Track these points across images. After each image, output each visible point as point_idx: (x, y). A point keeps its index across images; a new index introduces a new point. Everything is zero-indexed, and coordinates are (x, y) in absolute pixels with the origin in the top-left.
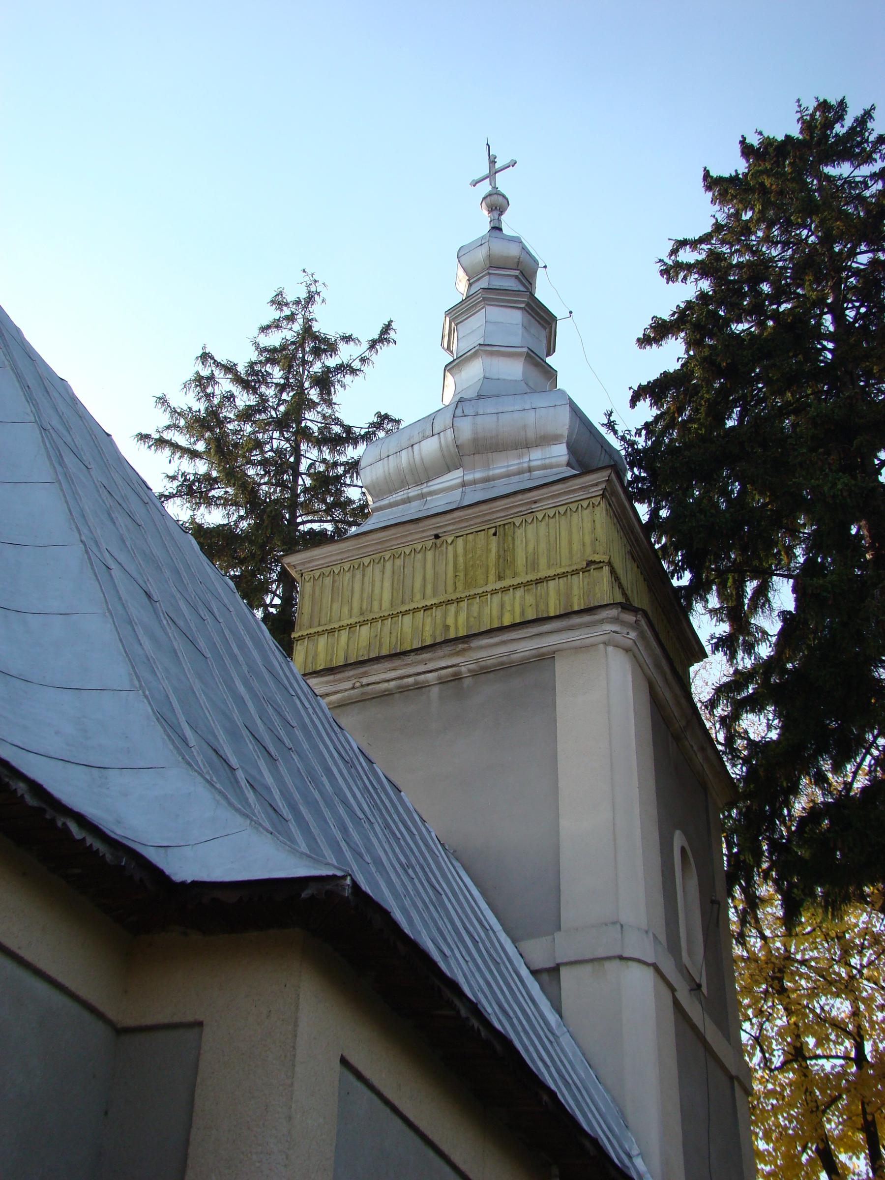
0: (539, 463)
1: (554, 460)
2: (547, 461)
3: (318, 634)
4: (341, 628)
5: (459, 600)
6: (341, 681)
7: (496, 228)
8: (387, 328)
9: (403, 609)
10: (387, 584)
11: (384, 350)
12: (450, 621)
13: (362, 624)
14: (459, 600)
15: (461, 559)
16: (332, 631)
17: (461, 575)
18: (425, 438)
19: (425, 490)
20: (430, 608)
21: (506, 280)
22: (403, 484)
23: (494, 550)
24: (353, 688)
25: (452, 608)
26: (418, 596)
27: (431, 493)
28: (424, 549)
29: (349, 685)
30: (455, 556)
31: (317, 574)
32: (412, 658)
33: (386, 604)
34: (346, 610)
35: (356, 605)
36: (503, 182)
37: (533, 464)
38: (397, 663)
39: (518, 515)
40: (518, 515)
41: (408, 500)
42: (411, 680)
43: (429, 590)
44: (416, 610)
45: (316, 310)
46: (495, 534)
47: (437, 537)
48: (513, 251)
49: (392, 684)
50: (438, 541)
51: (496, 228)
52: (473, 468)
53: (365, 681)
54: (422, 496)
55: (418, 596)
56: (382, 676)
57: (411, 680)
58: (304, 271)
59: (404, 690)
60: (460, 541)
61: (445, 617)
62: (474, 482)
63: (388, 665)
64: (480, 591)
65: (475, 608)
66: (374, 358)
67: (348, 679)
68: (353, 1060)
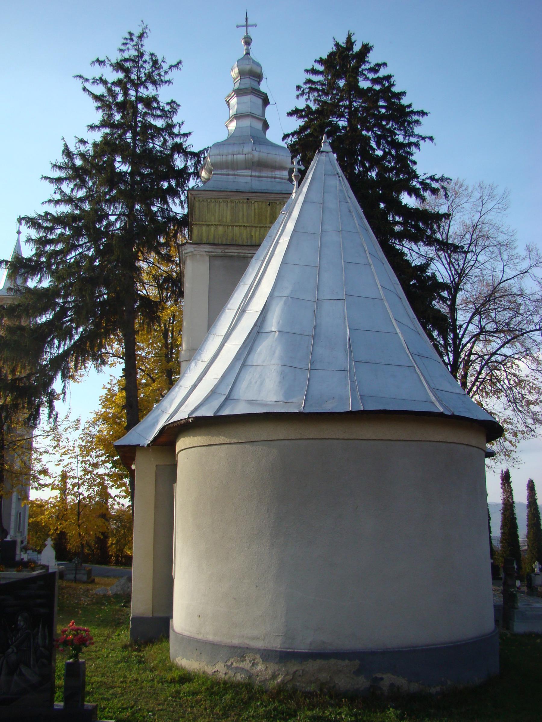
0: (279, 176)
1: (284, 177)
2: (281, 176)
3: (203, 225)
4: (212, 225)
5: (256, 227)
6: (217, 249)
7: (248, 54)
8: (179, 63)
9: (236, 224)
10: (229, 213)
11: (174, 70)
12: (253, 234)
13: (220, 225)
14: (256, 227)
15: (257, 211)
16: (208, 225)
17: (257, 217)
18: (239, 154)
19: (236, 173)
20: (246, 227)
21: (251, 80)
22: (227, 168)
23: (269, 211)
24: (222, 252)
25: (254, 229)
26: (241, 221)
27: (238, 175)
28: (243, 203)
29: (220, 251)
30: (255, 209)
31: (201, 200)
32: (245, 247)
33: (229, 220)
34: (213, 218)
35: (216, 217)
36: (252, 32)
37: (277, 176)
38: (239, 248)
39: (278, 200)
40: (278, 200)
41: (228, 175)
42: (243, 254)
43: (245, 219)
44: (240, 226)
45: (145, 41)
46: (269, 205)
47: (248, 199)
48: (259, 71)
49: (236, 254)
50: (248, 201)
51: (248, 54)
52: (255, 171)
53: (226, 251)
54: (234, 175)
55: (241, 221)
56: (233, 251)
57: (243, 254)
58: (142, 21)
59: (239, 257)
60: (256, 204)
61: (251, 231)
62: (255, 176)
63: (236, 248)
64: (264, 226)
65: (262, 231)
66: (170, 72)
67: (220, 249)
68: (513, 479)
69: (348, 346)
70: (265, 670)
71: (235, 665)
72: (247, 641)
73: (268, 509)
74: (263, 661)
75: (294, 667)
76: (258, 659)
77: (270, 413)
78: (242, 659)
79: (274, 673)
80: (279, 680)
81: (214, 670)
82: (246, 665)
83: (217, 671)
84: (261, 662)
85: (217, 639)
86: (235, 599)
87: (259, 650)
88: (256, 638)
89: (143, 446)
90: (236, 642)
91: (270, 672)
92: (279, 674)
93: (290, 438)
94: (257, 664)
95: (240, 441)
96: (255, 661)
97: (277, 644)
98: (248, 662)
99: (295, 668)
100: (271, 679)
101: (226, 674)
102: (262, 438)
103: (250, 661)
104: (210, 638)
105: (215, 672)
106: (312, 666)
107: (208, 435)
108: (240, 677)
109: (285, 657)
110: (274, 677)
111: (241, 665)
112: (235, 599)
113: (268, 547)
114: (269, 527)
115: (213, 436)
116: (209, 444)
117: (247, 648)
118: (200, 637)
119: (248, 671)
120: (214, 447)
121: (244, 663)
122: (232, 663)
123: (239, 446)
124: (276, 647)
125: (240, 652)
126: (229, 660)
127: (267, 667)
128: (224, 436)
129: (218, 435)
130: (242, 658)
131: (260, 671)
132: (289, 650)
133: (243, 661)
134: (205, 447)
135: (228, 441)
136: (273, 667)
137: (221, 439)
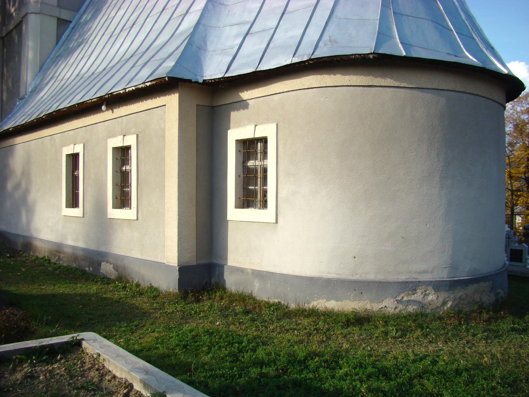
69: (463, 17)
70: (437, 299)
71: (405, 298)
72: (415, 276)
73: (438, 154)
74: (435, 291)
75: (460, 293)
76: (430, 290)
77: (443, 61)
78: (414, 292)
79: (445, 300)
80: (449, 306)
81: (380, 307)
82: (418, 296)
83: (385, 307)
84: (433, 292)
85: (381, 277)
86: (403, 238)
87: (431, 282)
88: (424, 272)
89: (197, 82)
90: (403, 278)
91: (441, 300)
92: (448, 301)
93: (457, 90)
94: (428, 295)
95: (410, 86)
96: (427, 292)
97: (443, 275)
98: (419, 294)
99: (460, 294)
100: (441, 306)
101: (395, 308)
102: (433, 87)
103: (422, 293)
104: (371, 277)
105: (382, 308)
106: (471, 289)
107: (369, 75)
108: (411, 309)
109: (452, 285)
110: (444, 303)
111: (413, 298)
112: (403, 238)
113: (437, 189)
114: (439, 170)
115: (377, 77)
116: (370, 84)
117: (419, 282)
118: (356, 277)
119: (420, 302)
120: (374, 88)
121: (415, 295)
122: (403, 298)
123: (408, 91)
124: (443, 278)
125: (411, 286)
126: (400, 295)
127: (438, 296)
128: (391, 78)
129: (383, 76)
130: (414, 291)
131: (432, 301)
132: (456, 279)
133: (413, 294)
134: (361, 88)
135: (397, 84)
136: (443, 295)
137: (388, 82)
